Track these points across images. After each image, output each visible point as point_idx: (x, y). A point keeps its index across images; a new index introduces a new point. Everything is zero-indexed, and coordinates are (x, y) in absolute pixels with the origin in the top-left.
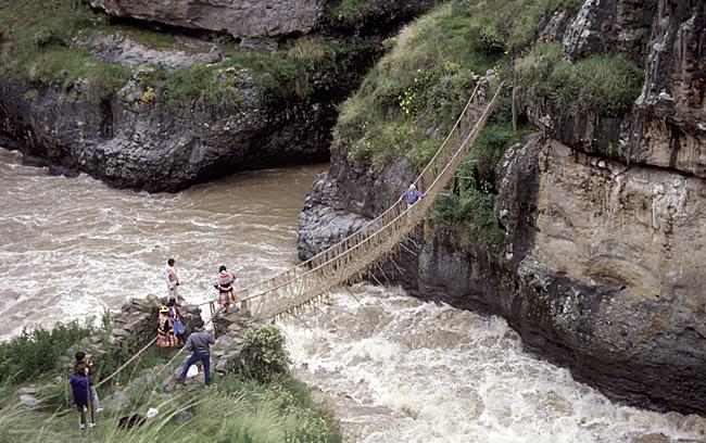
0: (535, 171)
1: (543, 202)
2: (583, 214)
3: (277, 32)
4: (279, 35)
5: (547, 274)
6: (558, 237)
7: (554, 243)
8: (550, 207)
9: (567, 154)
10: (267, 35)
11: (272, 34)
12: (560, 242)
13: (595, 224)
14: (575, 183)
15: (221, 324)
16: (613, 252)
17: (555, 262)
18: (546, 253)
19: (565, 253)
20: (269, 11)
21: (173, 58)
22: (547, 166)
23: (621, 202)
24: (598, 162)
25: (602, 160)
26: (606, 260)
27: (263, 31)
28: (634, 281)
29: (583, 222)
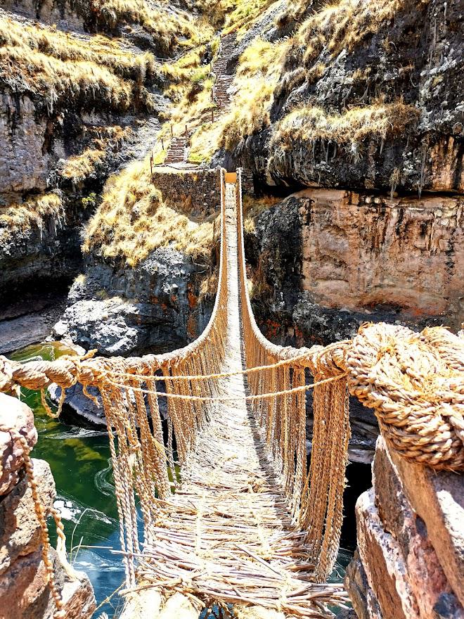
0: (297, 225)
1: (309, 250)
2: (355, 252)
3: (20, 188)
4: (22, 191)
5: (323, 312)
6: (327, 279)
7: (322, 285)
8: (318, 252)
9: (342, 196)
10: (13, 190)
11: (17, 189)
12: (328, 283)
13: (368, 259)
14: (350, 223)
15: (119, 7)
16: (386, 282)
17: (327, 300)
18: (315, 295)
19: (335, 292)
20: (12, 172)
21: (425, 496)
22: (309, 217)
23: (398, 232)
24: (373, 199)
25: (376, 197)
26: (378, 289)
27: (9, 187)
28: (407, 304)
29: (356, 259)
